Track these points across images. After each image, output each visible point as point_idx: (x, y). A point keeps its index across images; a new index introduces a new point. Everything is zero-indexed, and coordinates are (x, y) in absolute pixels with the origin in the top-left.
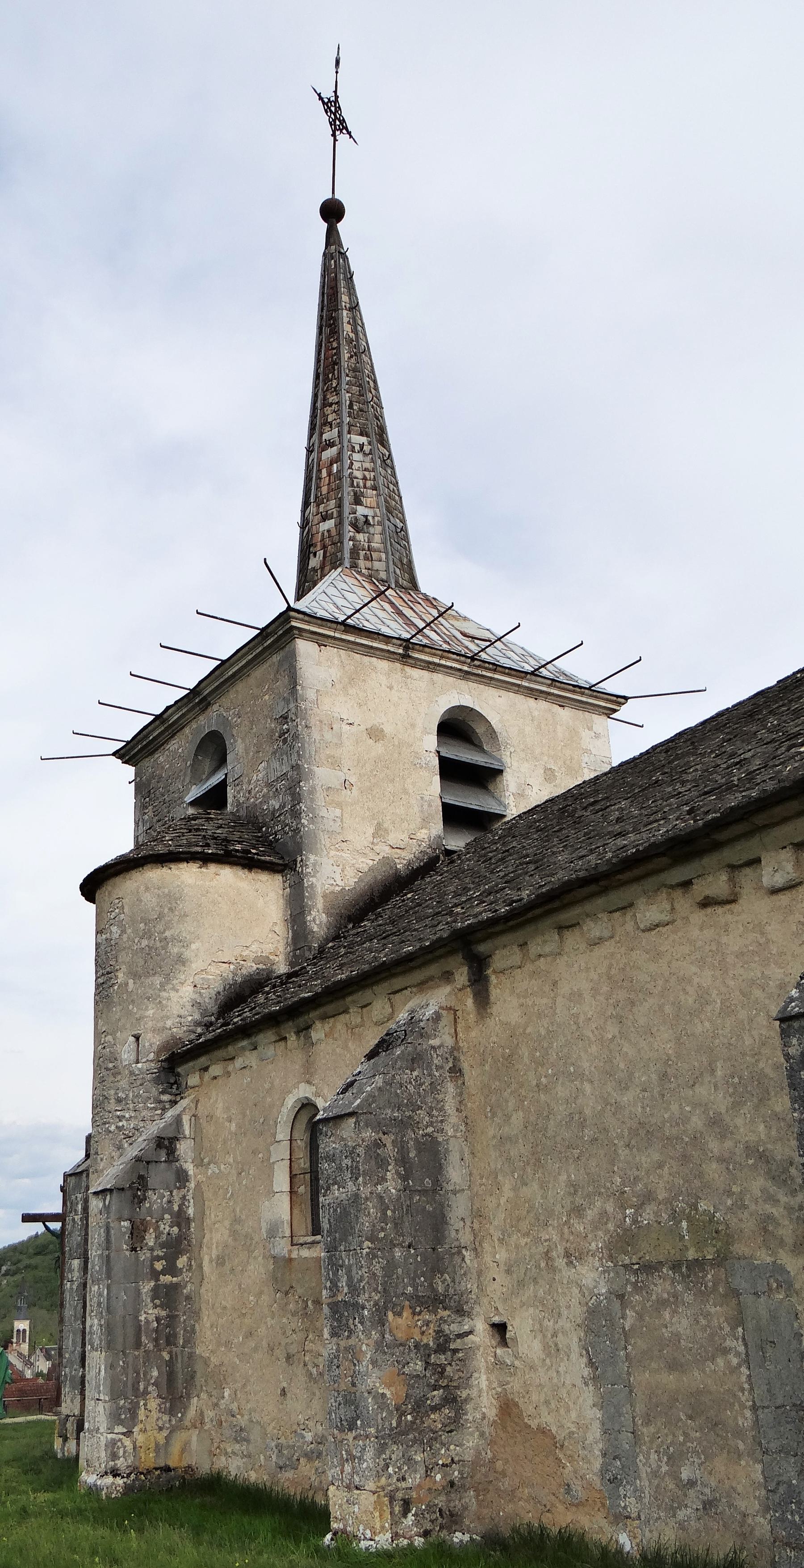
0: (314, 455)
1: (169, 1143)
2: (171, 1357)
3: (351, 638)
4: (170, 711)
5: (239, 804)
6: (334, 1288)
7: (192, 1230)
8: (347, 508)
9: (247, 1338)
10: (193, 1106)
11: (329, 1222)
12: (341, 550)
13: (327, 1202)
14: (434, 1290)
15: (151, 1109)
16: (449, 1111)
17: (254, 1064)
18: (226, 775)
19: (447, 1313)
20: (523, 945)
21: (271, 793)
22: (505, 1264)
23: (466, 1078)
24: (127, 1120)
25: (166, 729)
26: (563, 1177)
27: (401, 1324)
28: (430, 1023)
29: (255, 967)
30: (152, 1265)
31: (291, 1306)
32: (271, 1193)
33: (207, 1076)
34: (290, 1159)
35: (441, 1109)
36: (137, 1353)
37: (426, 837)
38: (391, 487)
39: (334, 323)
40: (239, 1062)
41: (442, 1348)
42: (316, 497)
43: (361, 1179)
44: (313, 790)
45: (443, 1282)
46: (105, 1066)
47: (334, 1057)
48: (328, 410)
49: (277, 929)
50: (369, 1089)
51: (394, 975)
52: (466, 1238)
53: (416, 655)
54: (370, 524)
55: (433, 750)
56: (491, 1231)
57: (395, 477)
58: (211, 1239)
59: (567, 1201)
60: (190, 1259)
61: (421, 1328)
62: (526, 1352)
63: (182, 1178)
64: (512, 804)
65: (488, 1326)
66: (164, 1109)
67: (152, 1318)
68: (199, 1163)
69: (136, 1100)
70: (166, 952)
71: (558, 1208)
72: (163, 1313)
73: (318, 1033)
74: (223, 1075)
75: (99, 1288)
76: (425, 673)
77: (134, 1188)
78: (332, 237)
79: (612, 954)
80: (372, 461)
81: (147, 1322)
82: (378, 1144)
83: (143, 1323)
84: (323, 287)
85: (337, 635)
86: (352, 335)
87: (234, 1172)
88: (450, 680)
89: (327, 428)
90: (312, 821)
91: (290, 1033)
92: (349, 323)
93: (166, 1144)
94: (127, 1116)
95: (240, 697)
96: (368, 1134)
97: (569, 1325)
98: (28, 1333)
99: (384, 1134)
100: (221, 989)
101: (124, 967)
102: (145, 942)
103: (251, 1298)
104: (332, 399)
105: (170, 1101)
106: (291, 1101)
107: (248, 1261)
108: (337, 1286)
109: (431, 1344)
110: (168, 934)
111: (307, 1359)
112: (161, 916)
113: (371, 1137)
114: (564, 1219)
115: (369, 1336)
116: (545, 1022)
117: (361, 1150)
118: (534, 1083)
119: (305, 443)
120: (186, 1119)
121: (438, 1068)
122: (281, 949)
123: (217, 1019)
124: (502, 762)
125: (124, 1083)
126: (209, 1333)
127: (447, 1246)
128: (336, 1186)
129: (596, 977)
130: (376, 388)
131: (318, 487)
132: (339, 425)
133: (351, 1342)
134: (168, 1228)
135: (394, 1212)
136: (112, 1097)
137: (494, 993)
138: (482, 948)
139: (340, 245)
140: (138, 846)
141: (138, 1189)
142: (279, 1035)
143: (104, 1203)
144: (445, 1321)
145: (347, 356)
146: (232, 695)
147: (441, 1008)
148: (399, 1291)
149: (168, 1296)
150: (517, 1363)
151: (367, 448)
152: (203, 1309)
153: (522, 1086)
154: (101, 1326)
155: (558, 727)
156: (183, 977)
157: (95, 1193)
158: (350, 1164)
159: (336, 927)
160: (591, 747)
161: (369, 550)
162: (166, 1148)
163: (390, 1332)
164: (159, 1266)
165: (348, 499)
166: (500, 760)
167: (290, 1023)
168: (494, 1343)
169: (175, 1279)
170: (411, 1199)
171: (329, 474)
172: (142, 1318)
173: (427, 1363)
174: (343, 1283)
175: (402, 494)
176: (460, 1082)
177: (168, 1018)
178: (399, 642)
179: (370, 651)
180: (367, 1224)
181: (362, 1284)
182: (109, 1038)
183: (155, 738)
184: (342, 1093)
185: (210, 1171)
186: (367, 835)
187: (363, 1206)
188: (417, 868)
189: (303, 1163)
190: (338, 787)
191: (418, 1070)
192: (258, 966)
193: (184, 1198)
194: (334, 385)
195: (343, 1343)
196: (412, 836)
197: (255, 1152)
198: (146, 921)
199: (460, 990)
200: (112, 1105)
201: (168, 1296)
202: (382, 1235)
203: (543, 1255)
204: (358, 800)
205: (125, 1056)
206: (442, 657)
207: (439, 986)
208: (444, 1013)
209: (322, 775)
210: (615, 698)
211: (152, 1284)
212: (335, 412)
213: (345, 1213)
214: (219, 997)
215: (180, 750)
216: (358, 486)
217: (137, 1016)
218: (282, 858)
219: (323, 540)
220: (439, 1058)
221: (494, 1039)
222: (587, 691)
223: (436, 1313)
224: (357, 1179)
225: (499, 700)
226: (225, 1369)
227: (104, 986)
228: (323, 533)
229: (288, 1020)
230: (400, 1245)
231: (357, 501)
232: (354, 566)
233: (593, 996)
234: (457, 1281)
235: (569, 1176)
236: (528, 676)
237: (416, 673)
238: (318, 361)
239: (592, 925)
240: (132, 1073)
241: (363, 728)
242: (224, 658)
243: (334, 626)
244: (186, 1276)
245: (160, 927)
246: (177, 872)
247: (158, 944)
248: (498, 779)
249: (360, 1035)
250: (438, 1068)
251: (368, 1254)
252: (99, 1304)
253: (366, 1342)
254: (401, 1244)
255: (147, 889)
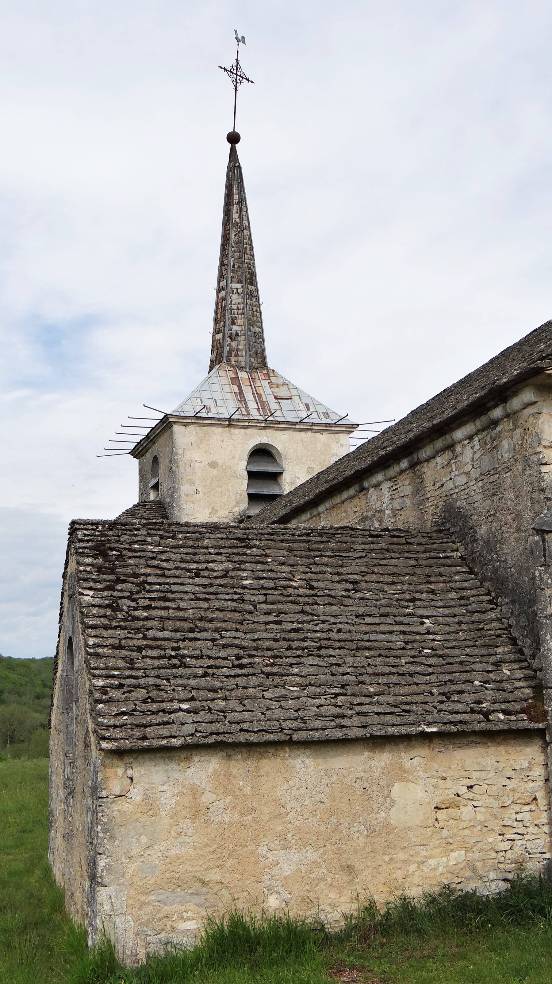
16: (191, 645)
44: (179, 497)
53: (236, 423)
85: (193, 421)
88: (256, 431)
92: (237, 213)
132: (227, 278)
145: (234, 234)
161: (237, 350)
216: (234, 314)
225: (283, 437)
231: (233, 323)
232: (228, 360)
241: (207, 463)
242: (153, 426)
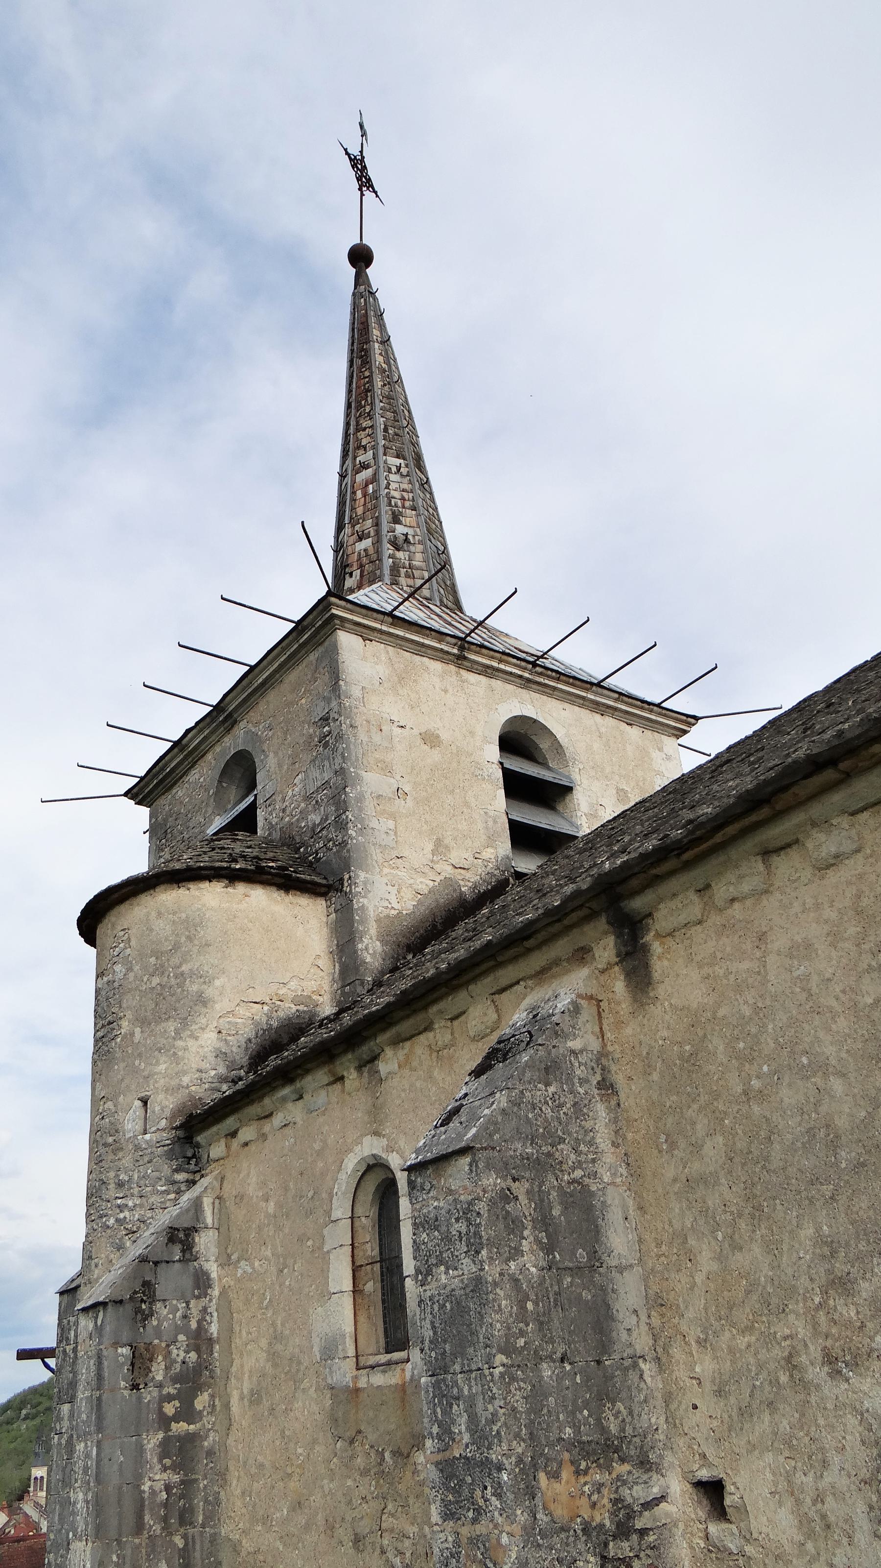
0: (348, 479)
1: (186, 1235)
2: (186, 1544)
3: (400, 633)
4: (190, 735)
5: (271, 827)
6: (446, 1435)
7: (216, 1355)
8: (385, 526)
9: (294, 1510)
10: (217, 1184)
11: (433, 1327)
12: (380, 568)
13: (429, 1294)
14: (604, 1430)
15: (163, 1192)
16: (602, 1146)
17: (298, 1120)
18: (256, 795)
19: (626, 1467)
20: (704, 889)
21: (310, 808)
22: (713, 1382)
23: (622, 1096)
24: (131, 1210)
25: (186, 758)
26: (808, 1231)
27: (560, 1491)
28: (567, 1017)
29: (294, 1008)
30: (160, 1408)
31: (360, 1461)
32: (326, 1295)
33: (235, 1144)
34: (352, 1245)
35: (591, 1143)
36: (137, 1541)
37: (492, 857)
38: (431, 510)
39: (365, 355)
40: (278, 1120)
41: (623, 1530)
42: (351, 518)
43: (484, 1252)
44: (360, 799)
45: (616, 1416)
46: (104, 1142)
47: (412, 1095)
48: (361, 435)
49: (320, 963)
50: (487, 1112)
51: (500, 965)
52: (642, 1342)
54: (410, 543)
55: (496, 762)
56: (684, 1328)
57: (434, 502)
58: (242, 1366)
59: (821, 1269)
60: (212, 1396)
61: (589, 1496)
62: (764, 1530)
63: (202, 1282)
64: (584, 824)
65: (689, 1486)
66: (179, 1192)
67: (159, 1486)
68: (226, 1261)
69: (142, 1183)
70: (183, 991)
71: (804, 1281)
72: (176, 1478)
73: (389, 1063)
74: (257, 1139)
75: (86, 1446)
77: (138, 1299)
79: (860, 877)
80: (410, 482)
81: (153, 1493)
82: (507, 1196)
83: (146, 1495)
84: (354, 323)
85: (384, 628)
86: (384, 365)
87: (273, 1269)
89: (361, 451)
90: (361, 831)
91: (348, 1069)
92: (381, 354)
93: (181, 1237)
94: (130, 1204)
95: (271, 706)
96: (491, 1181)
97: (845, 1481)
98: (45, 1480)
99: (514, 1180)
100: (252, 1035)
101: (129, 1015)
102: (156, 980)
103: (300, 1451)
104: (365, 423)
105: (187, 1181)
106: (351, 1163)
107: (293, 1397)
108: (451, 1432)
109: (607, 1523)
110: (185, 968)
111: (386, 1542)
112: (176, 947)
113: (495, 1185)
114: (817, 1300)
115: (511, 1519)
116: (750, 996)
117: (482, 1206)
118: (739, 1089)
119: (337, 469)
120: (207, 1202)
121: (583, 1081)
122: (326, 987)
123: (247, 1073)
124: (570, 779)
125: (127, 1161)
126: (239, 1503)
127: (616, 1356)
128: (442, 1268)
129: (833, 915)
130: (411, 417)
131: (353, 509)
133: (481, 1528)
134: (182, 1354)
135: (536, 1303)
136: (111, 1181)
137: (659, 966)
138: (637, 904)
139: (370, 286)
140: (150, 870)
141: (142, 1301)
142: (334, 1075)
143: (96, 1323)
144: (625, 1482)
145: (380, 384)
146: (262, 706)
147: (579, 996)
148: (553, 1437)
149: (182, 1453)
150: (749, 1549)
151: (404, 470)
152: (231, 1468)
153: (716, 1096)
154: (87, 1502)
155: (627, 745)
156: (204, 1021)
157: (85, 1310)
158: (464, 1230)
159: (393, 957)
160: (663, 769)
162: (181, 1242)
163: (545, 1508)
164: (169, 1409)
165: (385, 518)
166: (568, 777)
167: (350, 1056)
168: (702, 1514)
169: (192, 1427)
170: (559, 1282)
171: (365, 495)
172: (146, 1488)
173: (604, 1558)
174: (461, 1426)
175: (442, 519)
176: (613, 1103)
177: (185, 1073)
178: (453, 641)
179: (421, 649)
180: (498, 1325)
181: (495, 1428)
182: (109, 1105)
183: (173, 770)
184: (442, 1125)
185: (240, 1272)
186: (425, 852)
187: (491, 1296)
188: (485, 892)
189: (371, 1250)
190: (390, 795)
191: (554, 1084)
192: (298, 1007)
193: (204, 1310)
194: (367, 411)
195: (465, 1531)
196: (477, 855)
197: (301, 1240)
198: (158, 954)
199: (603, 972)
200: (112, 1192)
201: (182, 1453)
202: (521, 1342)
203: (783, 1362)
204: (414, 812)
205: (129, 1126)
206: (501, 661)
207: (568, 972)
208: (583, 1003)
209: (370, 782)
210: (685, 718)
211: (161, 1435)
212: (369, 435)
213: (460, 1309)
214: (249, 1045)
215: (202, 780)
216: (396, 506)
217: (146, 1073)
218: (325, 878)
219: (359, 558)
220: (582, 1068)
221: (665, 1033)
222: (655, 708)
223: (609, 1469)
224: (478, 1252)
226: (261, 1558)
227: (104, 1040)
228: (359, 553)
229: (345, 1052)
230: (550, 1357)
232: (395, 582)
233: (833, 945)
234: (636, 1412)
235: (818, 1230)
236: (594, 688)
237: (472, 677)
238: (349, 392)
239: (822, 837)
240: (137, 1148)
241: (416, 732)
242: (253, 663)
243: (381, 617)
244: (207, 1421)
245: (175, 960)
246: (197, 893)
247: (173, 981)
248: (568, 798)
249: (451, 1058)
250: (583, 1081)
251: (502, 1375)
252: (86, 1469)
253: (507, 1528)
254: (551, 1357)
255: (160, 914)
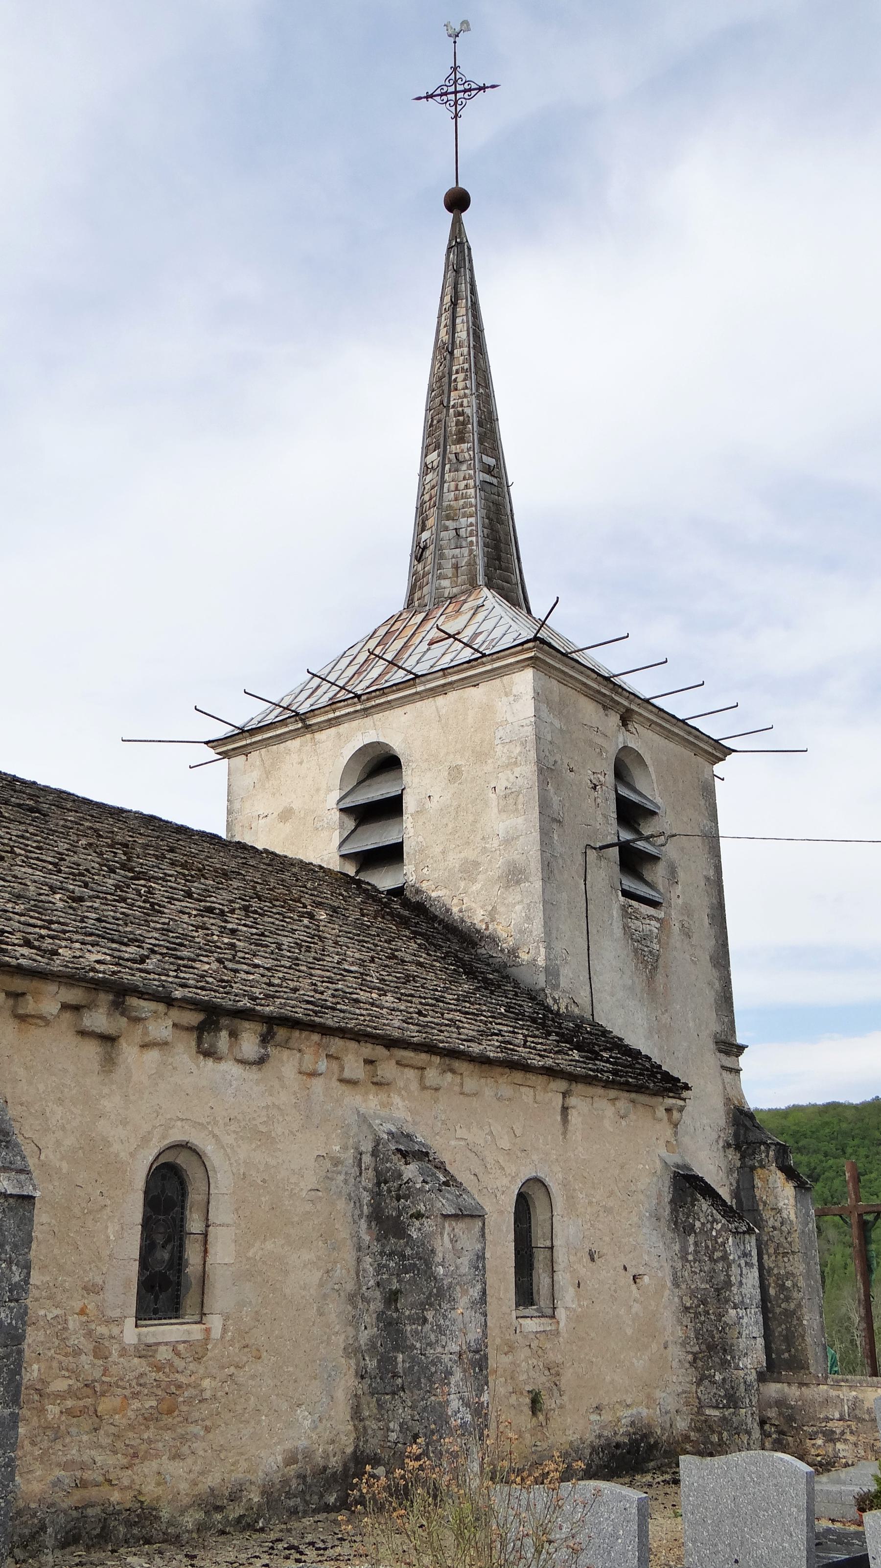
76: (333, 731)
78: (457, 229)
85: (249, 741)
88: (355, 724)
237: (321, 736)
241: (276, 814)
